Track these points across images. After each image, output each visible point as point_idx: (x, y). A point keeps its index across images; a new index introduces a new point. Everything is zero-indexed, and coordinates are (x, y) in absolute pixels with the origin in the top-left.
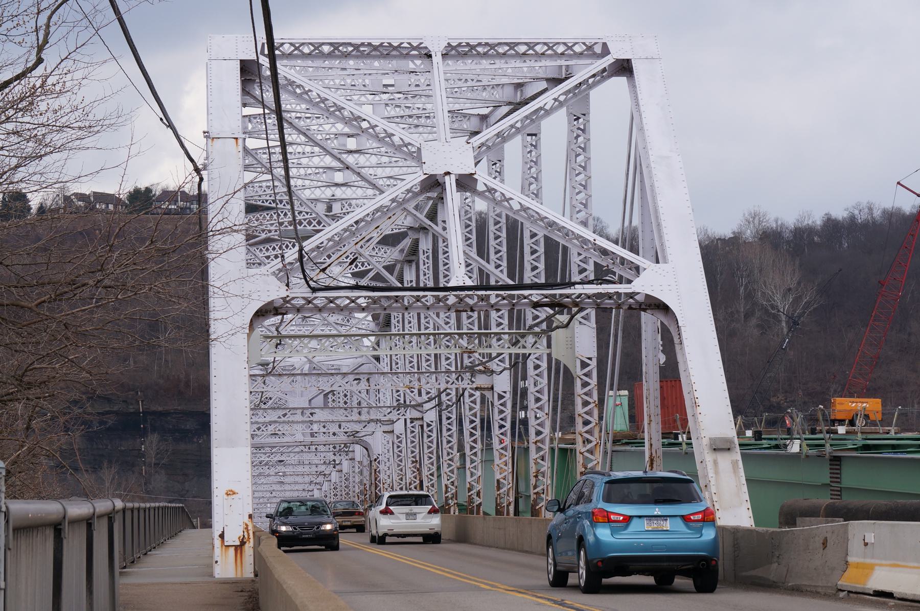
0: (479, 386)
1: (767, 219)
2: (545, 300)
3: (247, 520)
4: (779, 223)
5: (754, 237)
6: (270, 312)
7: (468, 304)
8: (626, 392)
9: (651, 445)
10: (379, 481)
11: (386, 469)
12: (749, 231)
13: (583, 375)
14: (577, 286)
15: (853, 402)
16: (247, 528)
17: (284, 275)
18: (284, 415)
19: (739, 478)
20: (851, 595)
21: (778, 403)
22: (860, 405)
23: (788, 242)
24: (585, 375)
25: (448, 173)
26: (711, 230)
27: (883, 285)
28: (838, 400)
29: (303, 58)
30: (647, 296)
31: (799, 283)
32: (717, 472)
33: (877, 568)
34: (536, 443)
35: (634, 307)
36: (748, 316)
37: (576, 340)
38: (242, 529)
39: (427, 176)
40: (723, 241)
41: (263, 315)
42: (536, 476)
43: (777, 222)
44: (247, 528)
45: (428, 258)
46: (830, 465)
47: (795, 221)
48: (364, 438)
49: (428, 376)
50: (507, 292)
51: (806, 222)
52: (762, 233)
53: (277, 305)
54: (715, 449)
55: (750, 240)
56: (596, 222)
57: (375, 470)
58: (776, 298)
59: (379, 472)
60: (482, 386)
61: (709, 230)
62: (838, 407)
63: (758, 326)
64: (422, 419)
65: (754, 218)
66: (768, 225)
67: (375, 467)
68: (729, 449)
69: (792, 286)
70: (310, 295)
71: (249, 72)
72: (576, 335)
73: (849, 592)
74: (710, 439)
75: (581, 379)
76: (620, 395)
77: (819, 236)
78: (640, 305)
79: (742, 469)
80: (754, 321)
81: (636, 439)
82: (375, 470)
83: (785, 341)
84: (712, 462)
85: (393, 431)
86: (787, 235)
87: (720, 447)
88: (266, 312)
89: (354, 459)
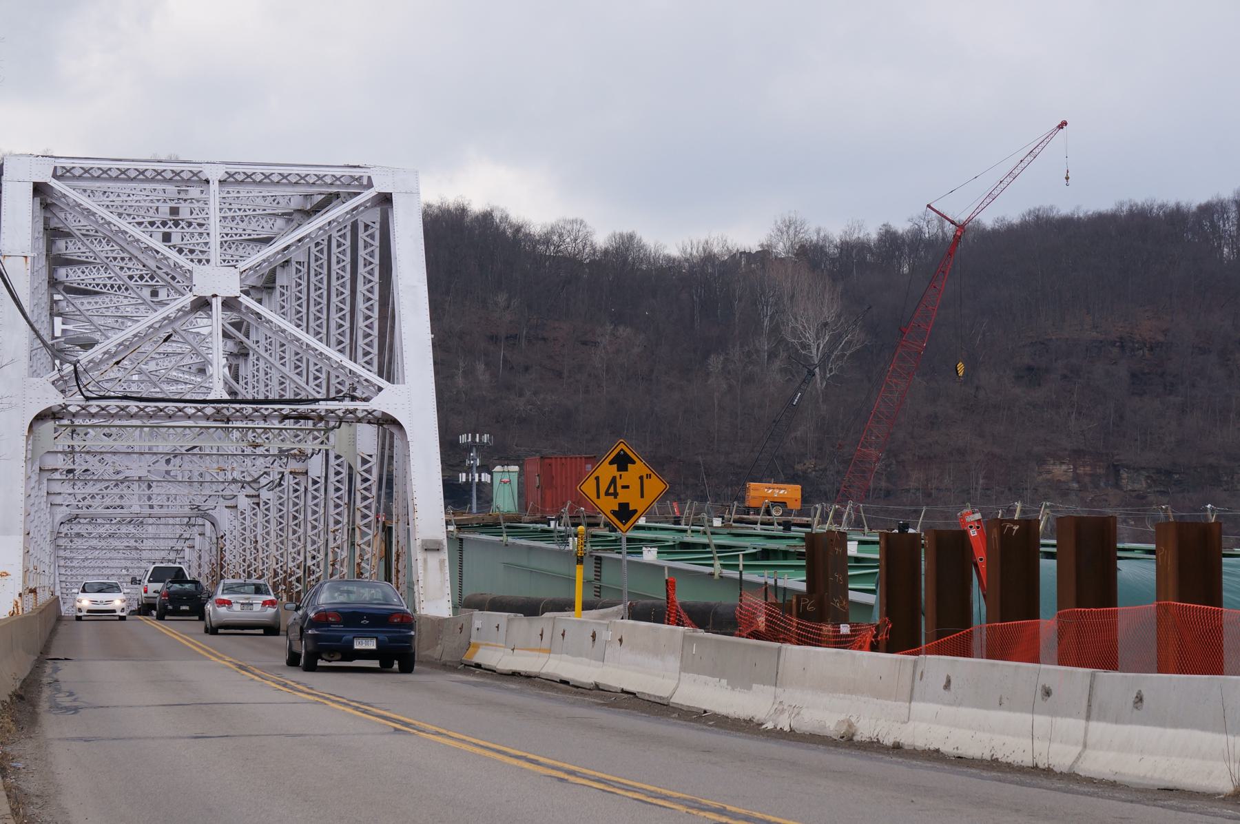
0: (293, 470)
1: (806, 228)
2: (293, 413)
3: (17, 597)
4: (822, 234)
5: (788, 252)
6: (49, 416)
7: (224, 415)
8: (516, 468)
9: (398, 542)
10: (225, 562)
11: (232, 548)
12: (781, 244)
13: (364, 471)
14: (321, 402)
15: (770, 488)
16: (16, 605)
17: (61, 385)
18: (106, 488)
19: (444, 575)
20: (466, 667)
21: (805, 472)
22: (777, 491)
23: (833, 260)
24: (366, 471)
25: (214, 296)
26: (732, 240)
27: (905, 334)
28: (753, 485)
29: (92, 180)
30: (383, 413)
31: (839, 316)
32: (425, 569)
33: (481, 647)
34: (334, 532)
35: (372, 421)
36: (772, 355)
37: (358, 437)
38: (12, 605)
39: (196, 297)
40: (748, 255)
41: (42, 419)
42: (333, 565)
43: (818, 234)
44: (16, 605)
45: (372, 254)
46: (596, 563)
47: (842, 233)
48: (210, 512)
49: (254, 459)
50: (258, 406)
51: (855, 236)
52: (799, 247)
53: (55, 410)
54: (426, 550)
55: (783, 255)
56: (579, 225)
57: (222, 549)
58: (808, 335)
59: (225, 551)
60: (297, 471)
61: (729, 241)
62: (752, 493)
63: (781, 370)
64: (259, 496)
65: (789, 227)
66: (807, 237)
67: (221, 545)
68: (438, 550)
69: (829, 320)
70: (83, 403)
71: (42, 192)
72: (358, 433)
73: (465, 665)
74: (422, 540)
75: (362, 475)
76: (509, 472)
77: (873, 254)
78: (378, 421)
79: (448, 567)
80: (777, 364)
81: (521, 523)
82: (222, 549)
83: (796, 395)
84: (422, 561)
85: (237, 506)
86: (832, 251)
87: (431, 547)
88: (45, 416)
89: (204, 534)
